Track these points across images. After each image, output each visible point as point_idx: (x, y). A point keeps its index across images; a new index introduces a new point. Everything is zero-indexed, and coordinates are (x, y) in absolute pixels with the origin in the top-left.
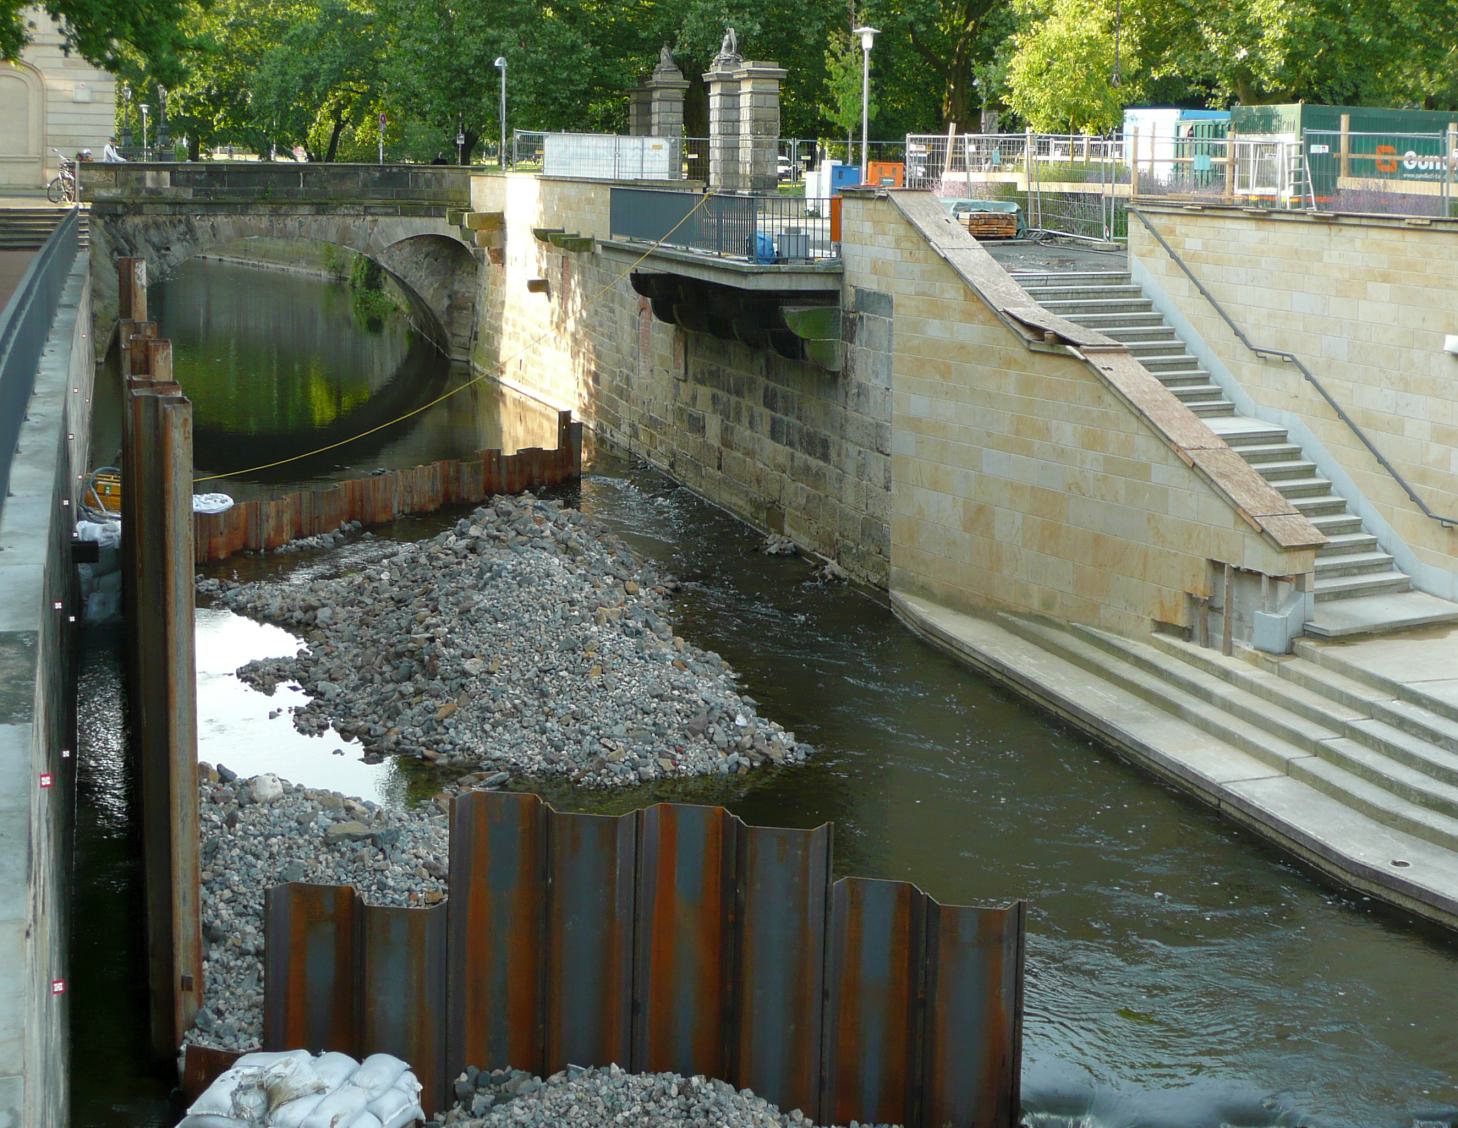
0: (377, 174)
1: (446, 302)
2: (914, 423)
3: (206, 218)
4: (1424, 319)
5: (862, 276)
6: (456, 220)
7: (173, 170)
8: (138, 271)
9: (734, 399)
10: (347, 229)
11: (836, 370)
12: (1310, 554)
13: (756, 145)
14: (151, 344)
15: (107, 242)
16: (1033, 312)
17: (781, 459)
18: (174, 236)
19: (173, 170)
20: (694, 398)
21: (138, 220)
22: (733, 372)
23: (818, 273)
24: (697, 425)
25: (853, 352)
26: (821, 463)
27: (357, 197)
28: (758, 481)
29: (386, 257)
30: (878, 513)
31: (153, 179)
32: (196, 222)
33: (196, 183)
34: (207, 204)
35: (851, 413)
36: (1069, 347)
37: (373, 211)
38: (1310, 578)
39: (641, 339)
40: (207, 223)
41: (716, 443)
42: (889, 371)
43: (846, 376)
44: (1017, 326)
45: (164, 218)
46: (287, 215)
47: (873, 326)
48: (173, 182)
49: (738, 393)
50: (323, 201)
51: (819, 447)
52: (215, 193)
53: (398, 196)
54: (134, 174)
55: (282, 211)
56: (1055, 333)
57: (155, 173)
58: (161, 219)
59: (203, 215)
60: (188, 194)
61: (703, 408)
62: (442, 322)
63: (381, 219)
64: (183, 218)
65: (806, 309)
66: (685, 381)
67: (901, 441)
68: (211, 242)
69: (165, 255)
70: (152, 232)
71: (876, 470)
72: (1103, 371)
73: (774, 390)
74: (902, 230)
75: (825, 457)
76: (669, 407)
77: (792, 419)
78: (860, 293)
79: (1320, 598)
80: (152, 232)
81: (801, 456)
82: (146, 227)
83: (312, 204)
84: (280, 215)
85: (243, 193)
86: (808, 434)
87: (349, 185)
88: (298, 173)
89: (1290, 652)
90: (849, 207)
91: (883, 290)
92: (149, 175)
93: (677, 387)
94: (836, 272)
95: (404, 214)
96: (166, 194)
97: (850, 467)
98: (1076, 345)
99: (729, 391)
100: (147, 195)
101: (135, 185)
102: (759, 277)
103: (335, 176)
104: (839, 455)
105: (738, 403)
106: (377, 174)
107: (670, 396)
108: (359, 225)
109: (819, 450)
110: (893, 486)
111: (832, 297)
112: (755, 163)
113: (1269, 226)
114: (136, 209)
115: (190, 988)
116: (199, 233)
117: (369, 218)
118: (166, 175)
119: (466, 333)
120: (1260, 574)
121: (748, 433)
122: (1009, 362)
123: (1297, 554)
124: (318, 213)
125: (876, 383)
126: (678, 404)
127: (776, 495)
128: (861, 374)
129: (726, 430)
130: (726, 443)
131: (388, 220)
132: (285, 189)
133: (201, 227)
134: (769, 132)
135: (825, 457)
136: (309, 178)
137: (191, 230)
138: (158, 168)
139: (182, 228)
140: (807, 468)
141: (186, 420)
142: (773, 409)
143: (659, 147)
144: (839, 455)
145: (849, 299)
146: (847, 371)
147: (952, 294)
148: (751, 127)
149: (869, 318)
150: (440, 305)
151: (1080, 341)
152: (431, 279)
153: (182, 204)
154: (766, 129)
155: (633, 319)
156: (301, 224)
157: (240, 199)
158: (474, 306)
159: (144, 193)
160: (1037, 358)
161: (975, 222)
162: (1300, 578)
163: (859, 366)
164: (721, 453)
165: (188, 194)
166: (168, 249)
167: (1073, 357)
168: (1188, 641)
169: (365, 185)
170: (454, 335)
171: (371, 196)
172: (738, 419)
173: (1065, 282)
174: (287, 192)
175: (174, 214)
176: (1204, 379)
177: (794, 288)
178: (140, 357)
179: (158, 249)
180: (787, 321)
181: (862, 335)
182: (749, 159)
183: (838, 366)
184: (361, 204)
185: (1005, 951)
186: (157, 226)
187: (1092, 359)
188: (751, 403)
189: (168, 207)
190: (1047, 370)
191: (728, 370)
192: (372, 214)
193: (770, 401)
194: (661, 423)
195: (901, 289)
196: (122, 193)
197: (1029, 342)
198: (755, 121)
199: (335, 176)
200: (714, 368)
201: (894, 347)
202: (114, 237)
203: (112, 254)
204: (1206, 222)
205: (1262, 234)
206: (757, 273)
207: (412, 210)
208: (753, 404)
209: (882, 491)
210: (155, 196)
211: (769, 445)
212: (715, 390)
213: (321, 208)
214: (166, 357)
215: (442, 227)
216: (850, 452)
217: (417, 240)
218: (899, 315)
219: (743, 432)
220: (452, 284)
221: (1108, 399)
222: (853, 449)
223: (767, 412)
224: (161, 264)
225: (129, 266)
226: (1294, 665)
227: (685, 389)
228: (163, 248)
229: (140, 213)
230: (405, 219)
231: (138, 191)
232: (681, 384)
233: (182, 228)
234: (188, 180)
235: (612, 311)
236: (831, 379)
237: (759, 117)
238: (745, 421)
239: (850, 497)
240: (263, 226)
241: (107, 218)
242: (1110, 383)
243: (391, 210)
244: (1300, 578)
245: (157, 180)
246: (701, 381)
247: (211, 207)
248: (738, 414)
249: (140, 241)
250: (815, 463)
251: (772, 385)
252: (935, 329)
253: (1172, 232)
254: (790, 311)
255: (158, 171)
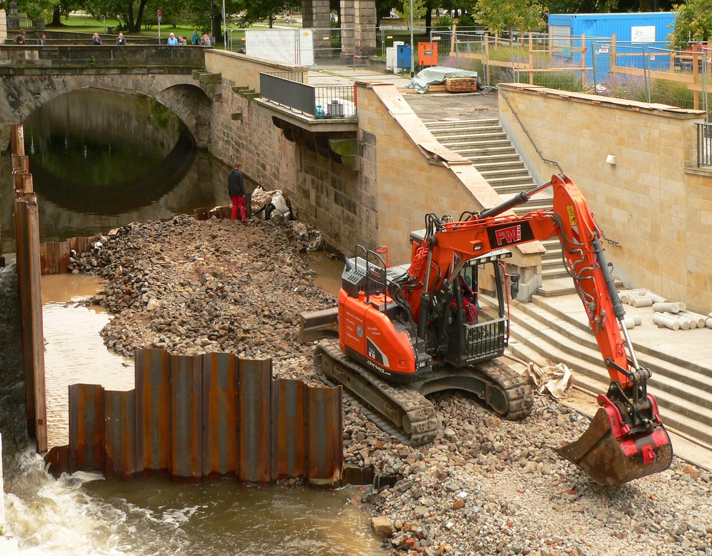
0: (154, 51)
1: (194, 122)
2: (386, 196)
3: (60, 77)
4: (601, 148)
5: (365, 126)
6: (196, 77)
7: (40, 49)
8: (19, 131)
9: (320, 182)
10: (138, 81)
11: (357, 170)
12: (539, 257)
13: (363, 31)
14: (24, 177)
15: (5, 90)
16: (433, 145)
17: (339, 213)
18: (42, 87)
19: (40, 49)
20: (305, 180)
21: (21, 78)
22: (320, 168)
23: (345, 123)
24: (306, 194)
25: (363, 162)
26: (354, 215)
27: (143, 64)
28: (331, 223)
29: (160, 96)
30: (374, 240)
31: (29, 55)
32: (54, 79)
33: (54, 57)
34: (61, 69)
35: (364, 191)
36: (444, 163)
37: (152, 71)
38: (539, 268)
39: (283, 148)
40: (60, 79)
41: (313, 203)
42: (376, 171)
43: (361, 173)
44: (423, 152)
45: (36, 77)
46: (105, 75)
47: (369, 149)
48: (40, 56)
49: (322, 179)
50: (124, 66)
51: (352, 207)
52: (64, 62)
53: (166, 63)
54: (18, 52)
55: (102, 72)
56: (438, 156)
57: (30, 51)
58: (34, 78)
59: (57, 75)
60: (49, 63)
61: (308, 186)
62: (193, 133)
63: (157, 76)
64: (47, 77)
65: (341, 140)
66: (301, 171)
67: (381, 205)
68: (63, 89)
69: (37, 97)
70: (30, 84)
71: (373, 220)
72: (457, 174)
73: (335, 178)
74: (378, 104)
75: (355, 213)
76: (295, 185)
77: (341, 193)
78: (364, 132)
79: (545, 277)
80: (30, 84)
81: (347, 212)
82: (27, 82)
83: (118, 68)
84: (101, 74)
85: (79, 62)
86: (349, 201)
87: (138, 57)
88: (109, 51)
89: (530, 301)
90: (359, 89)
91: (372, 133)
92: (27, 52)
93: (297, 175)
94: (354, 122)
95: (169, 73)
96: (37, 63)
97: (364, 217)
98: (446, 161)
99: (318, 178)
100: (26, 64)
101: (19, 58)
102: (317, 126)
103: (130, 51)
104: (360, 211)
105: (322, 184)
106: (154, 51)
107: (295, 179)
108: (145, 80)
109: (352, 209)
110: (379, 226)
111: (354, 134)
112: (363, 40)
113: (548, 100)
114: (20, 72)
115: (42, 424)
116: (56, 85)
117: (150, 75)
118: (36, 53)
119: (206, 139)
120: (517, 266)
121: (326, 199)
122: (422, 169)
123: (532, 257)
124: (121, 73)
125: (371, 177)
126: (299, 183)
127: (337, 231)
128: (366, 173)
129: (318, 197)
130: (318, 203)
131: (161, 76)
132: (103, 59)
133: (58, 82)
134: (370, 23)
135: (355, 213)
136: (116, 53)
137: (51, 83)
138: (32, 49)
139: (47, 82)
140: (349, 217)
141: (36, 212)
142: (335, 188)
143: (306, 35)
144: (360, 211)
145: (360, 136)
146: (361, 170)
147: (399, 136)
148: (360, 20)
149: (368, 146)
150: (191, 123)
151: (447, 160)
152: (186, 109)
153: (46, 69)
154: (369, 21)
155: (279, 137)
156: (112, 80)
157: (80, 66)
158: (209, 123)
159: (24, 63)
160: (433, 167)
161: (454, 84)
162: (535, 267)
163: (365, 169)
164: (316, 209)
165: (49, 63)
166: (39, 94)
167: (445, 167)
168: (493, 297)
169: (147, 57)
170: (200, 140)
171: (150, 62)
172: (322, 193)
173: (463, 126)
174: (104, 61)
175: (42, 75)
176: (526, 173)
177: (334, 130)
178: (19, 181)
179: (34, 94)
180: (332, 147)
181: (366, 154)
182: (359, 38)
183: (357, 168)
184: (145, 68)
185: (333, 403)
186: (33, 82)
187: (452, 168)
188: (327, 184)
189: (38, 71)
190: (435, 172)
191: (318, 167)
192: (152, 73)
193: (334, 184)
194: (292, 193)
195: (379, 132)
196: (12, 62)
197: (429, 159)
198: (362, 16)
199: (130, 51)
200: (312, 166)
201: (377, 160)
202: (8, 87)
203: (8, 97)
204: (526, 96)
205: (545, 104)
206: (316, 124)
207: (172, 71)
208: (327, 184)
209: (375, 229)
210: (31, 64)
211: (335, 206)
212: (313, 177)
213: (124, 70)
214: (30, 182)
215: (189, 80)
216: (363, 209)
217: (177, 87)
218: (379, 143)
219: (324, 199)
220: (198, 111)
221: (459, 187)
222: (365, 209)
223: (332, 188)
224: (36, 103)
225: (15, 128)
226: (531, 307)
227: (301, 175)
228: (36, 94)
229: (23, 74)
230: (170, 76)
231: (20, 62)
232: (300, 173)
233: (47, 82)
234: (49, 55)
235: (270, 133)
236: (355, 175)
237: (364, 14)
238: (325, 193)
239: (364, 232)
240: (91, 81)
241: (4, 77)
242: (459, 180)
243: (162, 71)
244: (535, 267)
245: (31, 55)
246: (307, 172)
247: (62, 71)
248: (322, 189)
249: (23, 89)
250: (351, 215)
251: (335, 175)
252: (393, 152)
253: (514, 100)
254: (333, 142)
255: (31, 50)
